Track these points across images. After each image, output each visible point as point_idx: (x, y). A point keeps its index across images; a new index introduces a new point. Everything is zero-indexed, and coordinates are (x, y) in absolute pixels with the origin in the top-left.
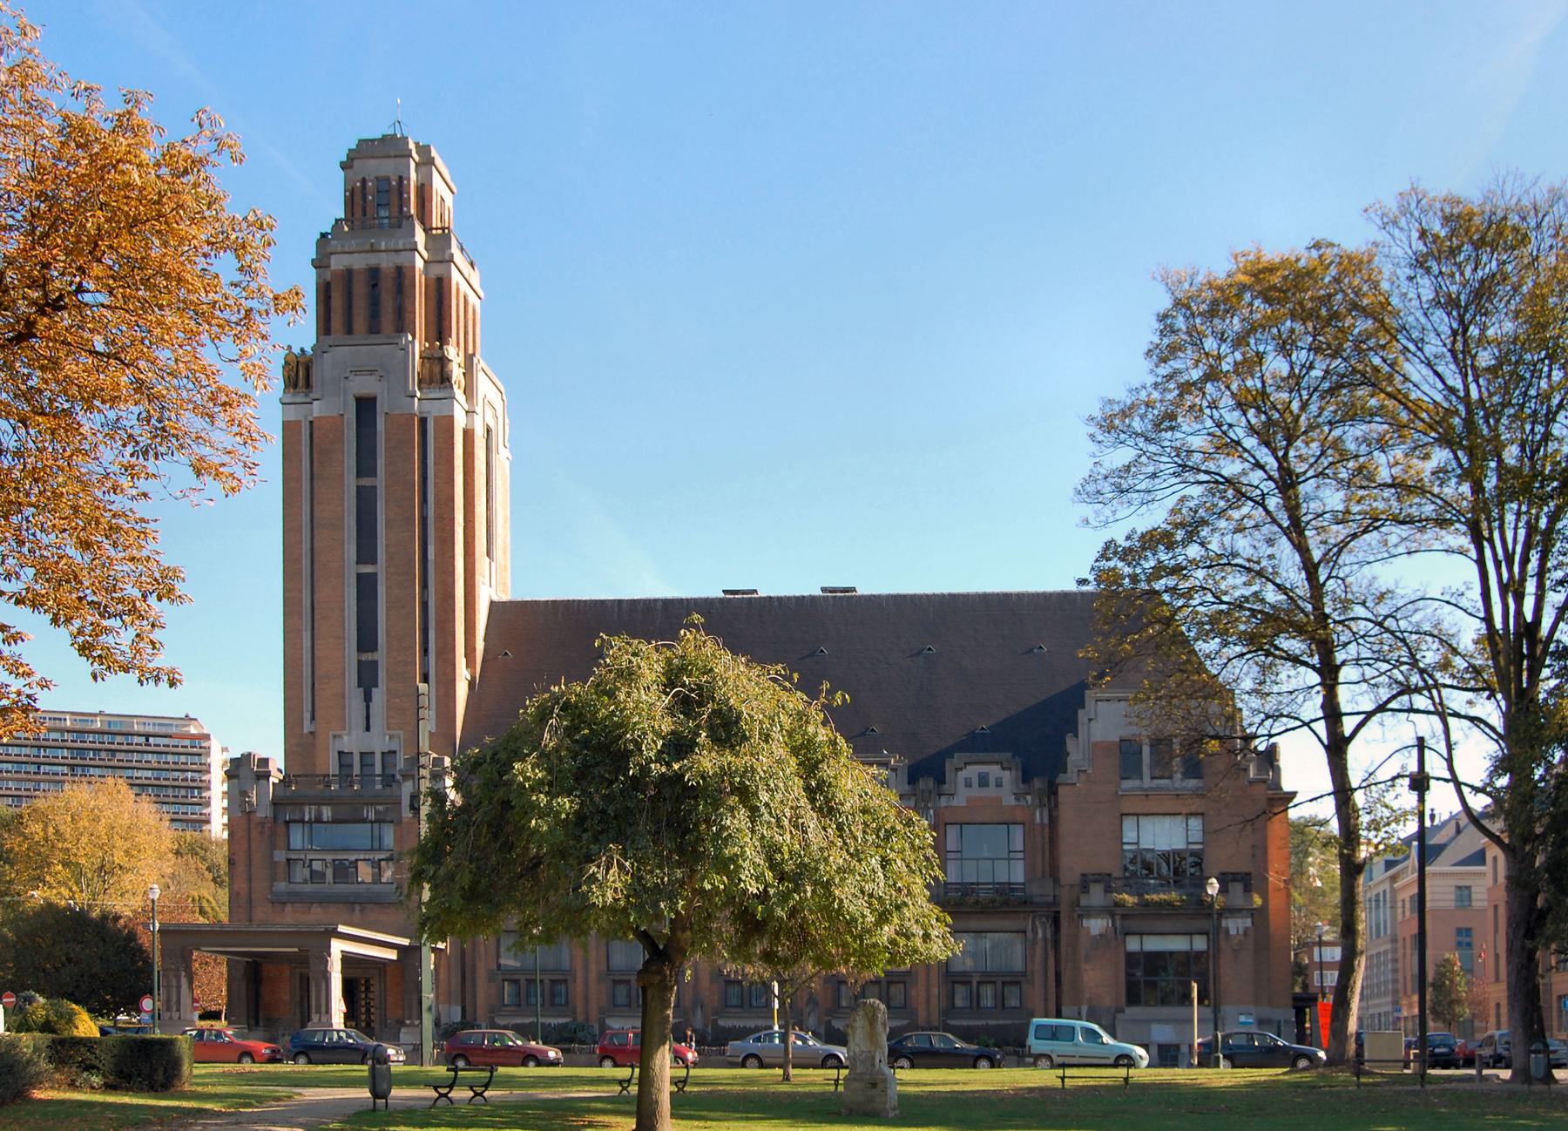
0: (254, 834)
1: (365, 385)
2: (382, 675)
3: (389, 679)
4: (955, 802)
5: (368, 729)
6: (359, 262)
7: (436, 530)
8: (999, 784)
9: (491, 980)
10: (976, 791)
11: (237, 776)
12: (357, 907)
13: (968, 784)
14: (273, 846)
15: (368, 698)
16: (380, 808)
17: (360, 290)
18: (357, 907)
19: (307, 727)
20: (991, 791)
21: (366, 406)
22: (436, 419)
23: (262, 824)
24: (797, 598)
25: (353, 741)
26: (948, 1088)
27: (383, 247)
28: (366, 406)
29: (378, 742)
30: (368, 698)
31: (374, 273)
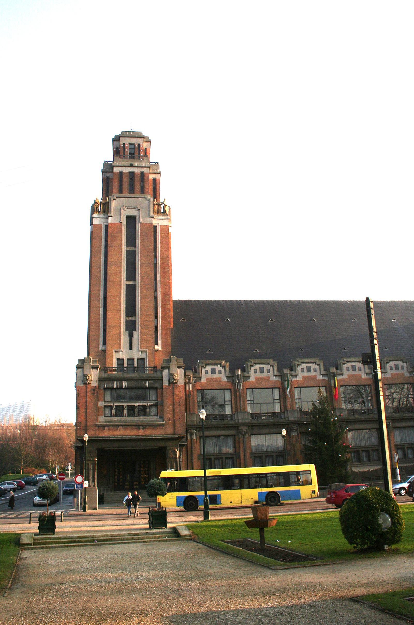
0: (89, 394)
1: (132, 212)
2: (138, 326)
3: (141, 328)
4: (298, 378)
5: (131, 348)
6: (126, 170)
7: (161, 268)
8: (403, 368)
9: (199, 459)
10: (351, 373)
11: (82, 368)
12: (141, 427)
13: (391, 368)
14: (98, 399)
15: (131, 336)
16: (151, 382)
17: (126, 180)
18: (141, 427)
19: (101, 347)
20: (400, 371)
21: (131, 220)
22: (161, 226)
23: (94, 389)
24: (284, 301)
25: (124, 354)
26: (124, 448)
27: (136, 165)
28: (131, 220)
29: (136, 354)
30: (131, 336)
31: (132, 174)
